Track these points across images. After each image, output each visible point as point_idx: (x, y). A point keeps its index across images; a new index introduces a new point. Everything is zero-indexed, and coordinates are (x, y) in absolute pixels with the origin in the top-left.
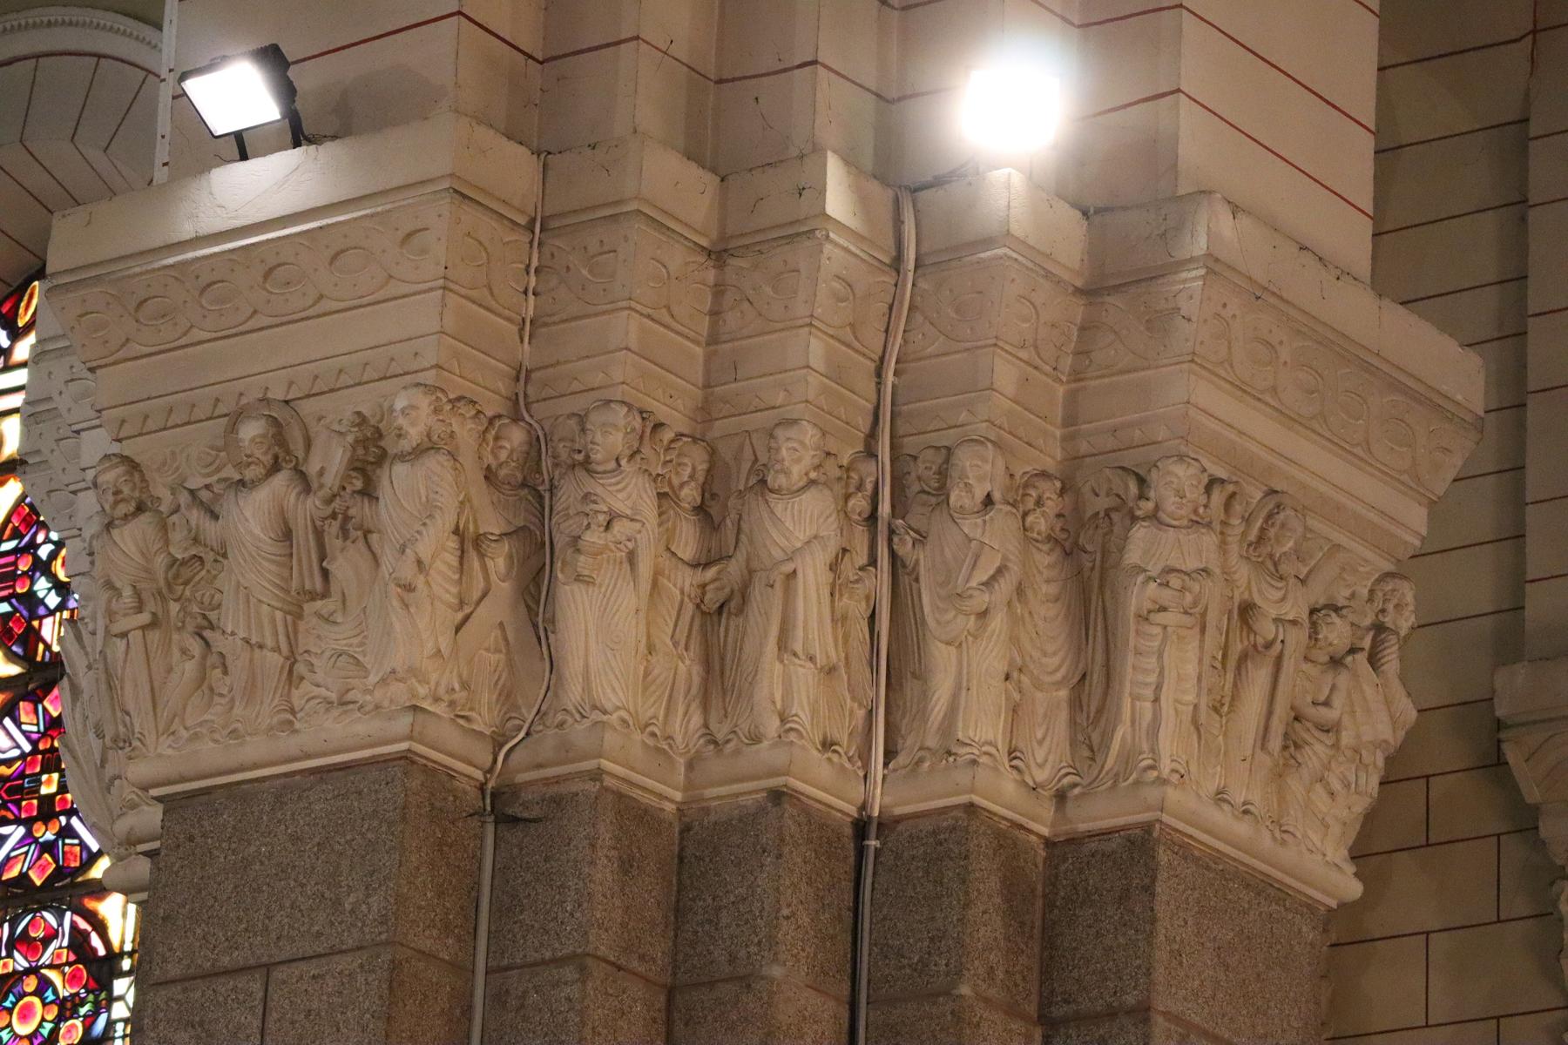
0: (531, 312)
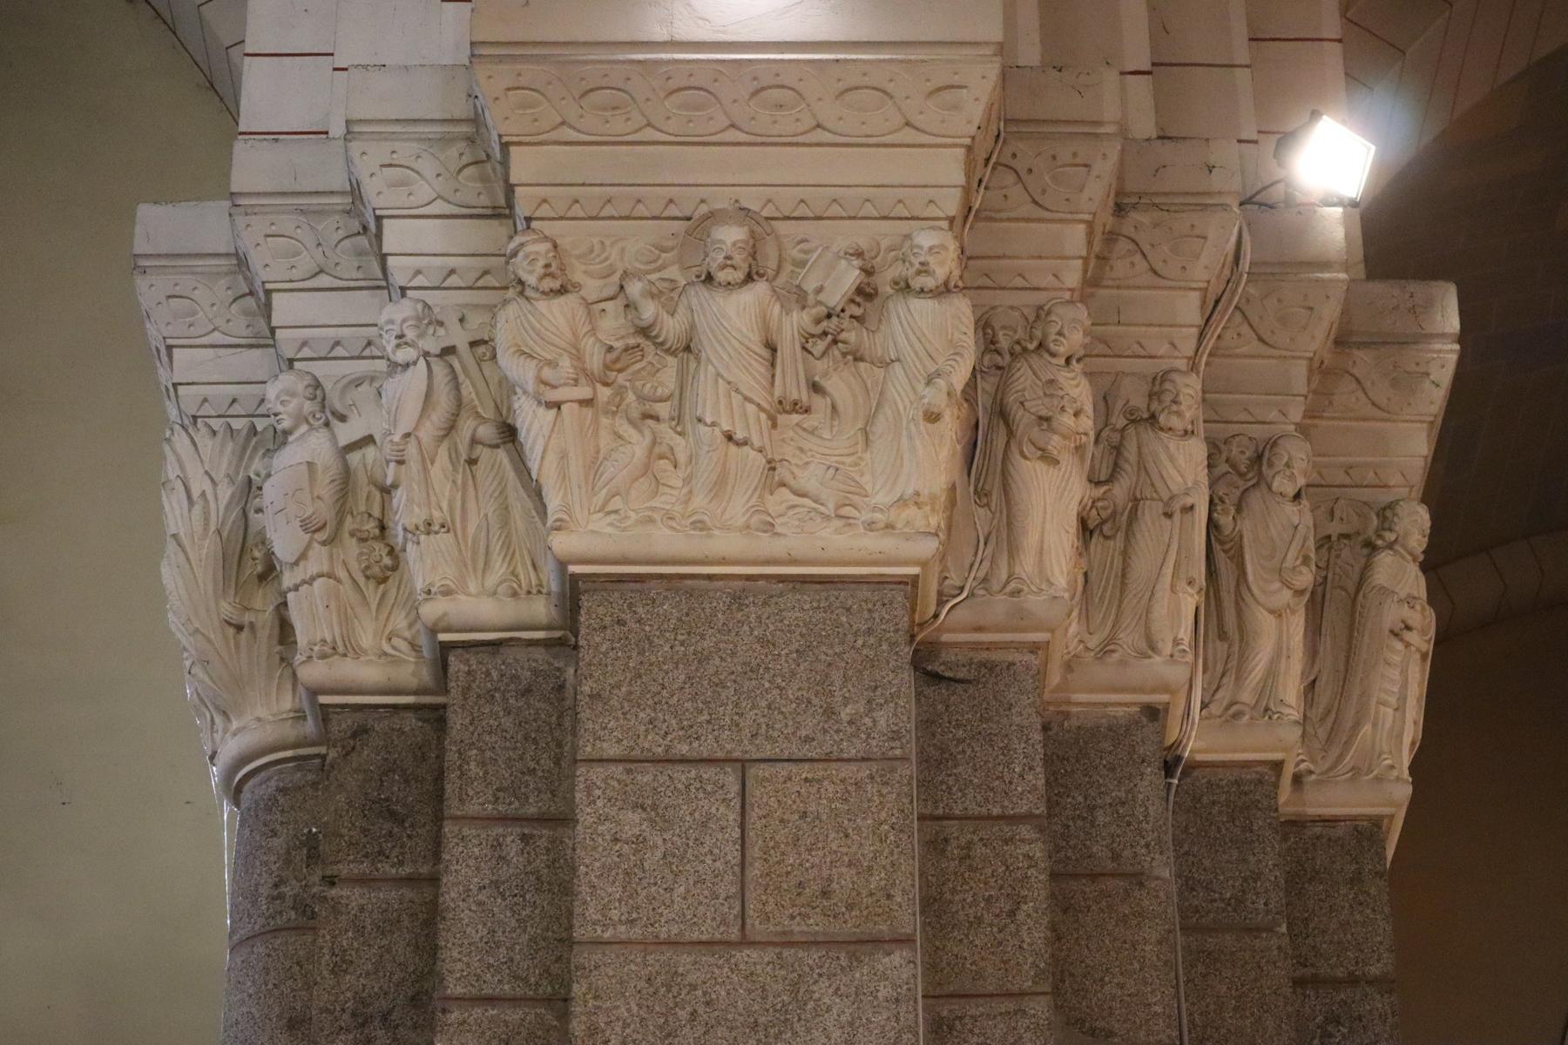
0: (977, 206)
